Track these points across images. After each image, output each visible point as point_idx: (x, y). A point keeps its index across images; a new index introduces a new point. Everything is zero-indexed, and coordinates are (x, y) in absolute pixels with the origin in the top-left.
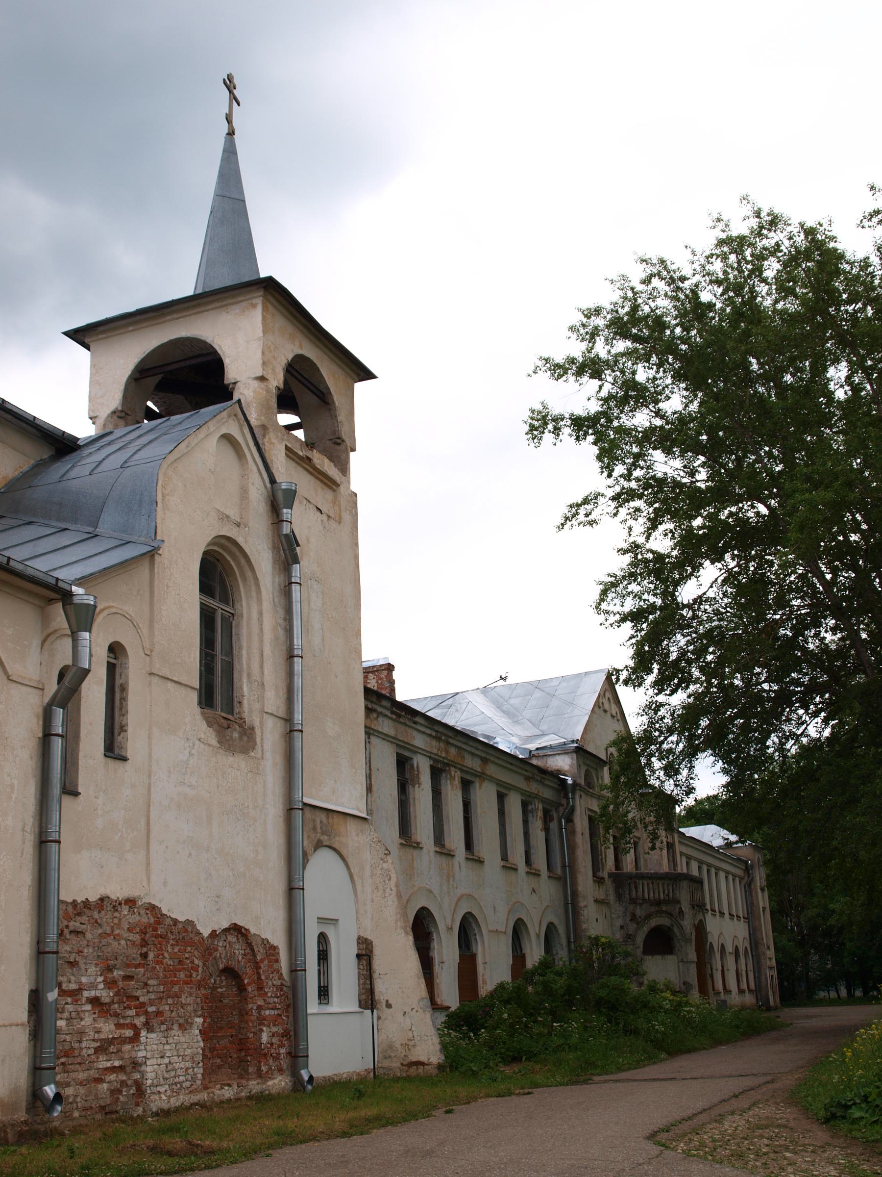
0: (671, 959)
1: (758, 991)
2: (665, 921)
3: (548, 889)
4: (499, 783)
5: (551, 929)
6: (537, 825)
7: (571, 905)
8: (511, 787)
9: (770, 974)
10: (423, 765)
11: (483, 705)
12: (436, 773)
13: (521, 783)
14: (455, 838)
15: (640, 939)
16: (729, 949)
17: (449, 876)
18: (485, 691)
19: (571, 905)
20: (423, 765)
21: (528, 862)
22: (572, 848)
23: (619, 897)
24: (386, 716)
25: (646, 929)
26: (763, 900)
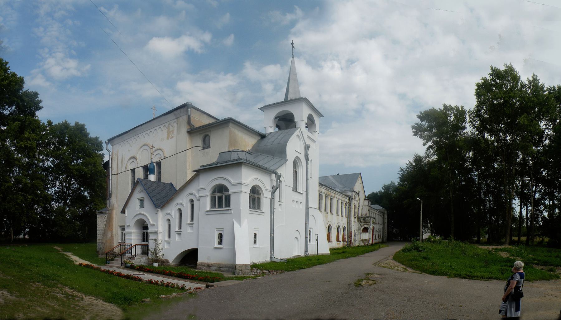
0: (367, 234)
1: (383, 239)
2: (367, 226)
3: (345, 220)
4: (337, 198)
5: (344, 227)
6: (344, 207)
7: (349, 223)
8: (339, 199)
9: (386, 236)
10: (323, 195)
11: (333, 180)
12: (326, 197)
13: (341, 198)
14: (340, 213)
15: (361, 229)
16: (342, 227)
17: (327, 217)
18: (333, 176)
19: (349, 223)
20: (323, 195)
21: (325, 210)
22: (350, 211)
23: (358, 221)
24: (384, 217)
25: (363, 227)
26: (386, 221)
